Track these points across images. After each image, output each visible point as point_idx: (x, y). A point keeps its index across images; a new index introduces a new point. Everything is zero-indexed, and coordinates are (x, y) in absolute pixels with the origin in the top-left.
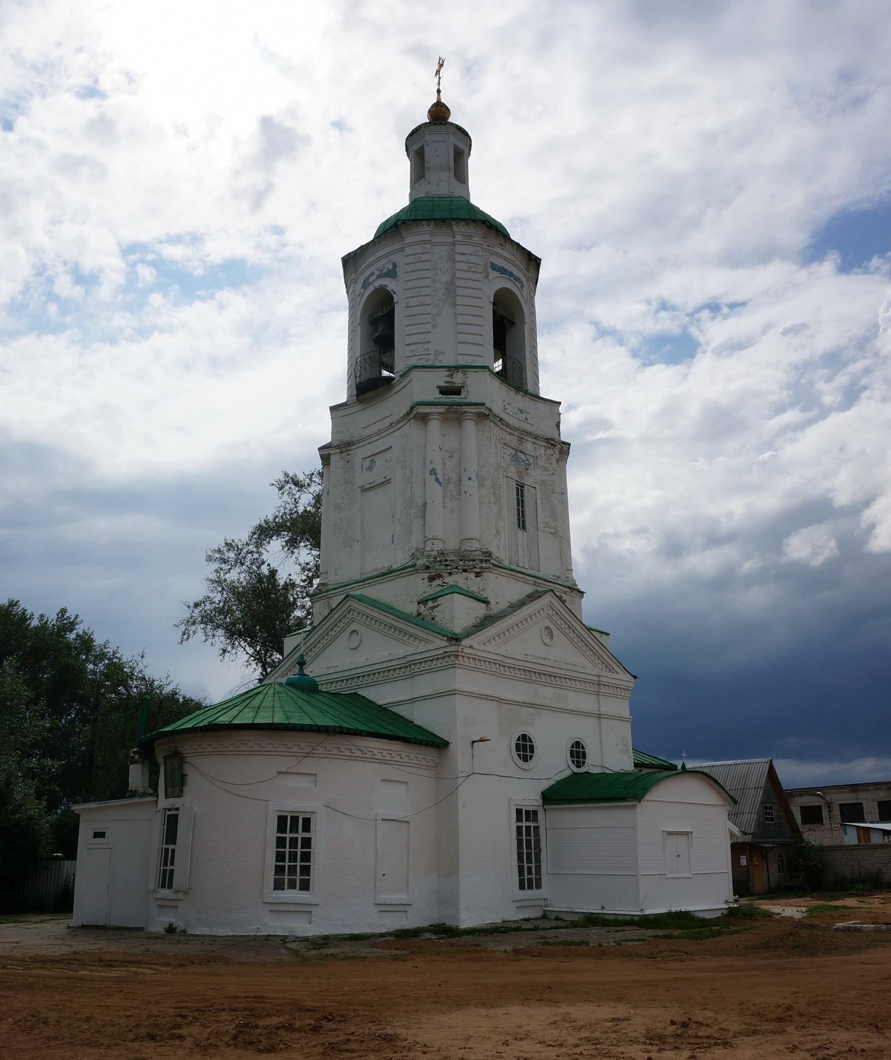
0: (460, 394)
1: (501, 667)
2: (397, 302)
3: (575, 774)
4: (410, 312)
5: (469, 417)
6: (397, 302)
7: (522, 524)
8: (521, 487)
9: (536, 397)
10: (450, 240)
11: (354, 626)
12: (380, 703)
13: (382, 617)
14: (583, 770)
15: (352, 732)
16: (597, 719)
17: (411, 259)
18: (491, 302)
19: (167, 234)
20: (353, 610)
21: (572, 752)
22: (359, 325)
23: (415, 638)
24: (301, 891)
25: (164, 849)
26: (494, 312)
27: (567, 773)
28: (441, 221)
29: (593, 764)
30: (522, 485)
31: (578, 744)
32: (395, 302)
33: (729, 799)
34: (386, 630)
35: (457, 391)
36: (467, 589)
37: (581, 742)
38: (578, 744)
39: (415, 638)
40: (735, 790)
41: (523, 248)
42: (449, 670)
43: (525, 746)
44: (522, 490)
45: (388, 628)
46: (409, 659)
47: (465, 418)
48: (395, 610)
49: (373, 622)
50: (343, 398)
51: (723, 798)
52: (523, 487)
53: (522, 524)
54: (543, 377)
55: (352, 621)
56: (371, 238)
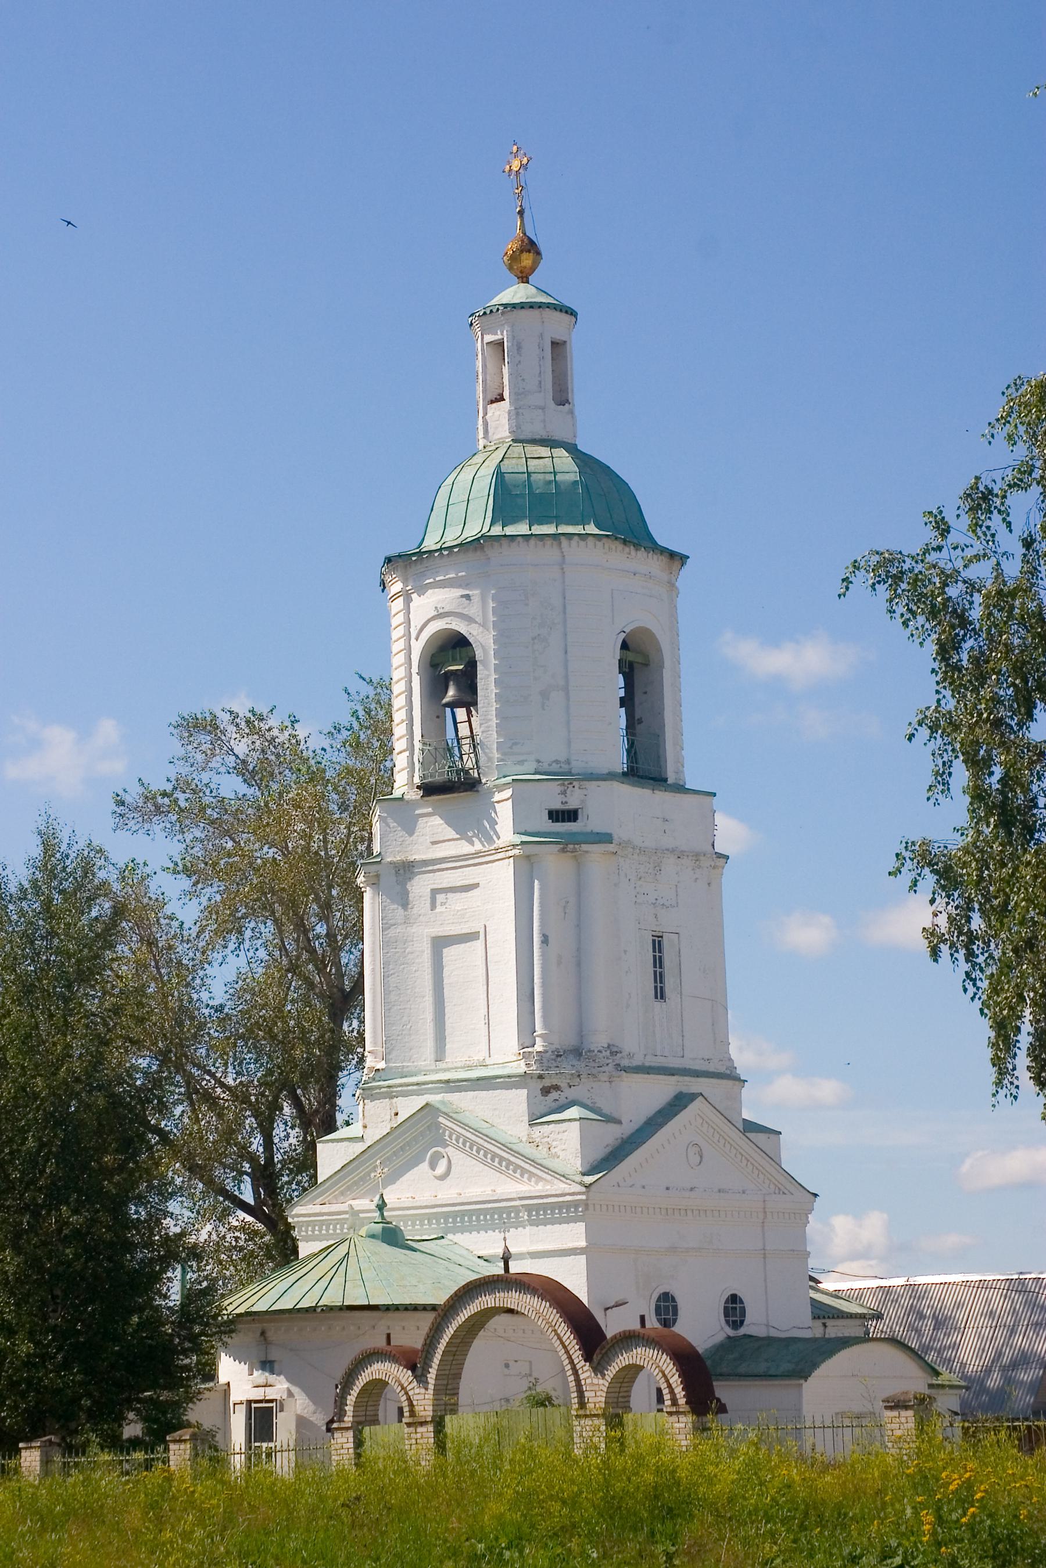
0: (575, 819)
3: (729, 1337)
7: (660, 994)
8: (659, 937)
9: (680, 788)
10: (559, 477)
14: (742, 1331)
16: (720, 1328)
21: (726, 1308)
24: (397, 1410)
25: (270, 1405)
27: (720, 1337)
29: (754, 1324)
30: (660, 934)
31: (734, 1299)
33: (930, 1370)
35: (571, 815)
36: (591, 1105)
37: (739, 1294)
38: (734, 1299)
40: (1021, 1291)
43: (667, 1308)
44: (659, 942)
51: (921, 1368)
52: (662, 937)
53: (660, 994)
54: (689, 754)
56: (497, 1318)
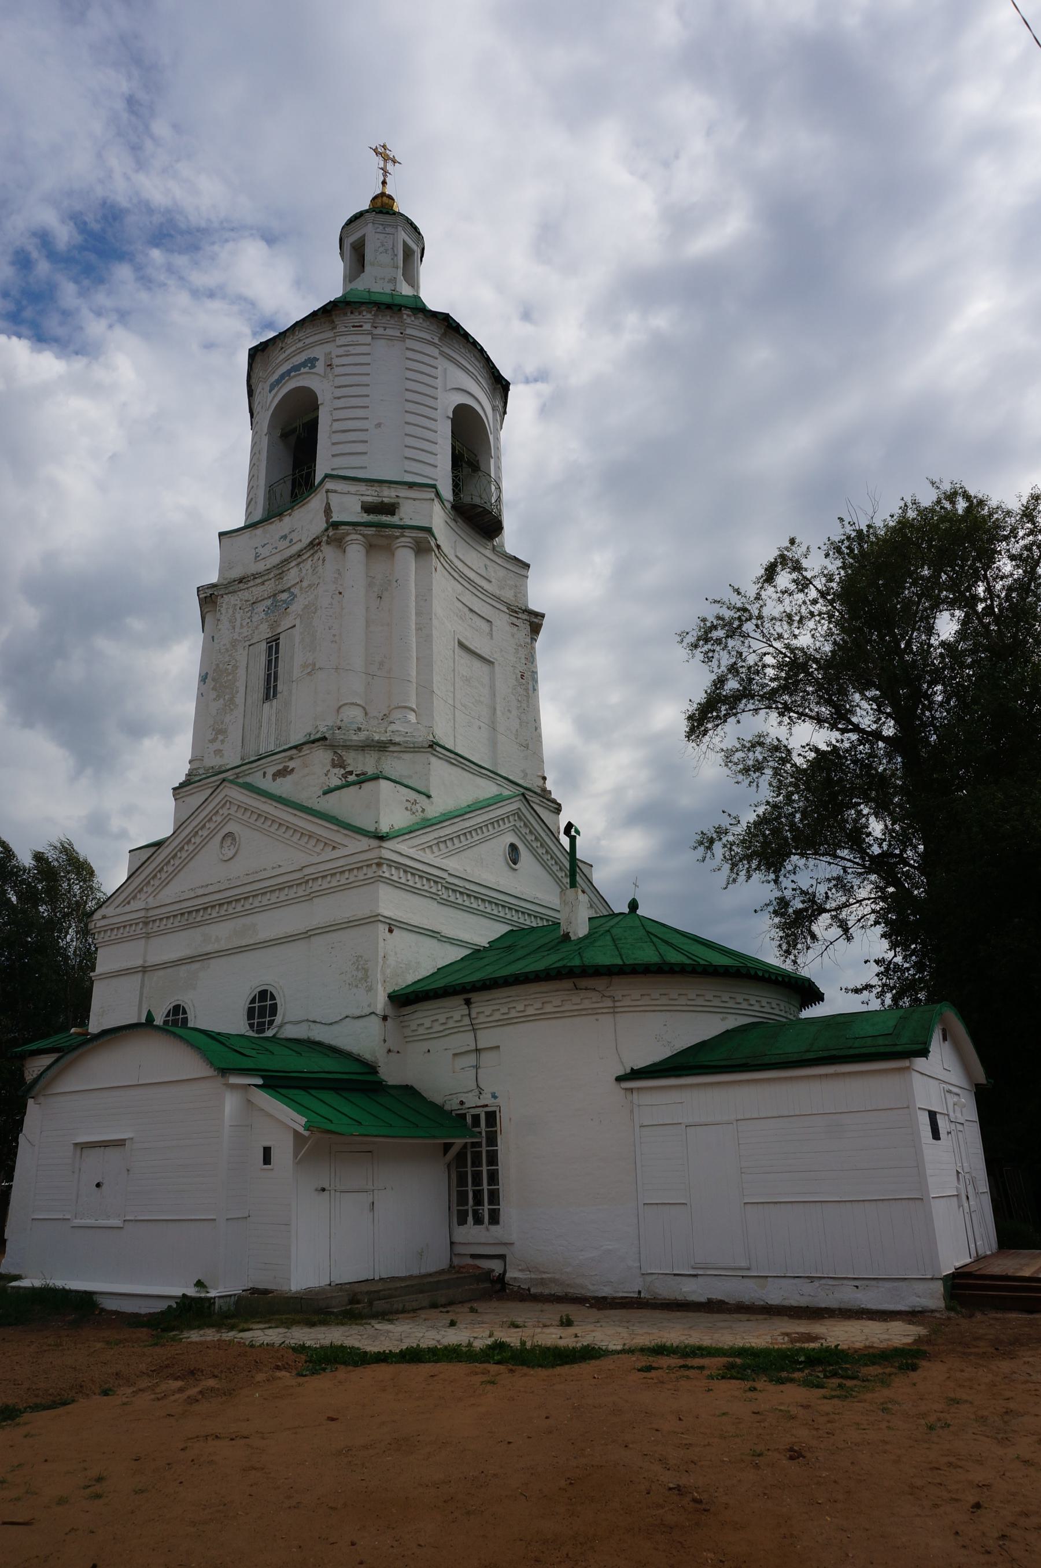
0: (393, 514)
1: (443, 888)
2: (322, 404)
4: (337, 426)
5: (403, 544)
6: (322, 404)
11: (231, 827)
12: (543, 968)
13: (256, 804)
15: (700, 969)
17: (341, 351)
18: (448, 417)
19: (632, 1069)
20: (230, 802)
22: (266, 435)
23: (310, 836)
26: (453, 448)
28: (385, 306)
32: (319, 403)
34: (252, 821)
39: (310, 836)
41: (494, 367)
42: (647, 1014)
45: (270, 823)
46: (306, 871)
47: (396, 546)
48: (433, 897)
49: (276, 826)
50: (238, 520)
55: (228, 819)
